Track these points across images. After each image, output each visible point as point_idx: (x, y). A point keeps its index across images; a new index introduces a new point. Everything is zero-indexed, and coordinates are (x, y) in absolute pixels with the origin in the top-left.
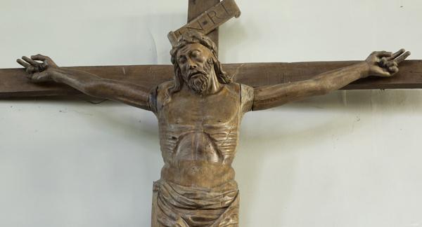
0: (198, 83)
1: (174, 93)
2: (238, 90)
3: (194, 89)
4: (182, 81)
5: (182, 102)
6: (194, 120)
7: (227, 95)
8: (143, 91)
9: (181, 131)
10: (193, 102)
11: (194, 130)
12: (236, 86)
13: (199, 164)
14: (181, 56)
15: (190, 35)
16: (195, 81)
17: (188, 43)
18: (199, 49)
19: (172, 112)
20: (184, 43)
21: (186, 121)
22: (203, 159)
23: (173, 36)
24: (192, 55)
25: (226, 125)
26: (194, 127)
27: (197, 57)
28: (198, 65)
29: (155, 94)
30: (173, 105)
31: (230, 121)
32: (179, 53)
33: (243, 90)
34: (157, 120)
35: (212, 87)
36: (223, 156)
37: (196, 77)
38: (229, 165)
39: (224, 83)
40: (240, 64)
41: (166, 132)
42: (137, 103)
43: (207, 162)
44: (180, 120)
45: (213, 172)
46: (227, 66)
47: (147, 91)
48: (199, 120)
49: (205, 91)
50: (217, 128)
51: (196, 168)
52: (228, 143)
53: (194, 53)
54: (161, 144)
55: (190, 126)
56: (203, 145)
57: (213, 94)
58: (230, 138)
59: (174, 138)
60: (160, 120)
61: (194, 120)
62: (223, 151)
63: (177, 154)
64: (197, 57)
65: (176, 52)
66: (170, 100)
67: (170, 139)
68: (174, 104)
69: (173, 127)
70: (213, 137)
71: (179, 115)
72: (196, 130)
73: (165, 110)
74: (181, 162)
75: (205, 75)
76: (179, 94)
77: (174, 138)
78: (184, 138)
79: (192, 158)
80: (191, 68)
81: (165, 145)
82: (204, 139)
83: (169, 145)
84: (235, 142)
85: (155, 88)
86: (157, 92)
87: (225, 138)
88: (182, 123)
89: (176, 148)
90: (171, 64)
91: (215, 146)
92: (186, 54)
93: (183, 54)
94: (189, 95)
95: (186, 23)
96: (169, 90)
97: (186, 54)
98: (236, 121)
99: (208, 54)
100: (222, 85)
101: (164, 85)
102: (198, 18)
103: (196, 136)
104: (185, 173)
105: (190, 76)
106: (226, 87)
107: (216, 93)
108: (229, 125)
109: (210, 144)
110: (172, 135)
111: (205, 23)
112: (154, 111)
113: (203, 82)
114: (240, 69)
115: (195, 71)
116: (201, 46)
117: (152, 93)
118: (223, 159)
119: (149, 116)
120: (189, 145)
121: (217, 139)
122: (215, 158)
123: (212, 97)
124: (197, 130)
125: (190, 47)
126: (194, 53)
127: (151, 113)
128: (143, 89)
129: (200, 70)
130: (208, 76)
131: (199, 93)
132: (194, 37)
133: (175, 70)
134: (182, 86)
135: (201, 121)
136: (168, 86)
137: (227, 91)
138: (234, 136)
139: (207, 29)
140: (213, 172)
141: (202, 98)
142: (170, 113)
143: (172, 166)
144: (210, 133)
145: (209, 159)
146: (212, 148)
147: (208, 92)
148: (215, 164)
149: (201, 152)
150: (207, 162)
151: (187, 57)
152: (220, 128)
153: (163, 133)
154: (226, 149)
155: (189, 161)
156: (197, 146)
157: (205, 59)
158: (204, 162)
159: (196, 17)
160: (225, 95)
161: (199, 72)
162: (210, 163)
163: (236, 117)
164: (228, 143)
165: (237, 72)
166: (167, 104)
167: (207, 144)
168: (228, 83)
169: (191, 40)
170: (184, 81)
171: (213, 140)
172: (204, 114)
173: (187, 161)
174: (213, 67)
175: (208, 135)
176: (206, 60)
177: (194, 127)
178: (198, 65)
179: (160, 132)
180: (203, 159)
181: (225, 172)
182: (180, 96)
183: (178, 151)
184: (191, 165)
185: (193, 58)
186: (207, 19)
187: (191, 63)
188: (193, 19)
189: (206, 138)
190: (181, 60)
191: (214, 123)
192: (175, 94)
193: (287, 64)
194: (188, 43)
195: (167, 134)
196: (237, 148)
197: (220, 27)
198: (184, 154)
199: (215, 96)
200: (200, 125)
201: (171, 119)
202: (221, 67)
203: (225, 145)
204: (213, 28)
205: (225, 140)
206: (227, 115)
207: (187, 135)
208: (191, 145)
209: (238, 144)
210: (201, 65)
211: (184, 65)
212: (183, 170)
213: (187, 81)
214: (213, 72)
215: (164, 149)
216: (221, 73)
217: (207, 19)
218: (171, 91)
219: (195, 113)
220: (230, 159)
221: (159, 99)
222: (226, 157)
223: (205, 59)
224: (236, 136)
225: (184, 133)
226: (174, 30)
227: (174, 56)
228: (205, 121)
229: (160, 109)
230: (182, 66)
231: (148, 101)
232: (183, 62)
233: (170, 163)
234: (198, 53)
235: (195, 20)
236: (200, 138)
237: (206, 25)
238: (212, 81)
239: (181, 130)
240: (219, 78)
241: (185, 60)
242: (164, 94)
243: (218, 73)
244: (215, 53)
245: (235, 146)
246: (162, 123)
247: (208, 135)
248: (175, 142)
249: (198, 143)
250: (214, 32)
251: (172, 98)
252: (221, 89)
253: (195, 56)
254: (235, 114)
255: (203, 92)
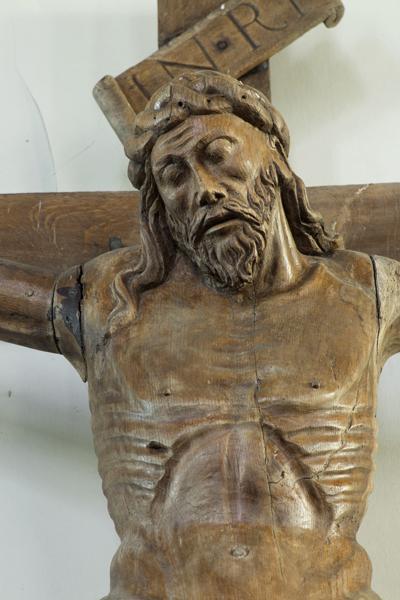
0: (231, 253)
1: (143, 290)
2: (368, 277)
3: (215, 276)
4: (169, 247)
5: (173, 322)
6: (222, 384)
7: (332, 293)
8: (31, 282)
9: (181, 424)
10: (212, 321)
11: (227, 417)
12: (358, 263)
13: (250, 537)
14: (169, 160)
15: (199, 86)
16: (221, 245)
17: (192, 112)
18: (231, 134)
19: (144, 355)
20: (178, 112)
21: (196, 385)
22: (261, 521)
23: (125, 92)
24: (207, 155)
25: (332, 397)
26: (225, 406)
27: (227, 163)
28: (229, 190)
29: (76, 293)
30: (145, 334)
31: (350, 384)
32: (160, 150)
33: (382, 275)
34: (83, 389)
35: (276, 265)
36: (330, 509)
37: (223, 233)
38: (350, 538)
39: (315, 254)
40: (352, 189)
41: (126, 426)
42: (11, 327)
43: (276, 530)
44: (174, 383)
45: (299, 564)
46: (336, 196)
47: (44, 282)
48: (241, 382)
49: (255, 282)
50: (306, 410)
51: (240, 551)
52: (345, 460)
53: (213, 146)
54: (103, 473)
55: (213, 403)
56: (263, 474)
57: (280, 292)
58: (353, 445)
59: (155, 448)
60: (97, 387)
61: (222, 384)
62: (329, 489)
63: (168, 503)
64: (227, 163)
65: (149, 148)
66: (130, 313)
67: (140, 451)
68: (146, 327)
69: (148, 408)
70: (291, 439)
71: (170, 366)
72: (233, 418)
73: (117, 348)
74: (186, 535)
75: (254, 223)
76: (159, 293)
77: (155, 448)
78: (195, 446)
79: (222, 515)
80: (206, 201)
81: (125, 472)
82: (264, 450)
83: (140, 474)
84: (368, 459)
85: (70, 271)
86: (81, 288)
87: (335, 446)
88: (185, 395)
89: (165, 483)
90: (129, 187)
91: (302, 472)
92: (187, 151)
93: (178, 153)
94: (197, 298)
95: (155, 47)
96: (125, 280)
97: (187, 151)
98: (367, 386)
99: (263, 149)
100: (309, 261)
101: (105, 263)
102: (197, 29)
103: (234, 439)
104: (204, 570)
105: (203, 229)
106: (325, 266)
107: (293, 288)
108: (348, 400)
109: (287, 467)
110: (145, 438)
111: (223, 45)
112: (70, 354)
113: (248, 249)
114: (354, 205)
115: (220, 211)
116: (239, 121)
117: (63, 291)
118: (331, 518)
119: (53, 370)
120: (213, 471)
121: (309, 449)
122: (303, 515)
123: (280, 301)
124: (236, 418)
125: (199, 128)
126: (213, 146)
127: (56, 365)
128: (32, 278)
129: (238, 209)
130: (264, 227)
131: (232, 288)
132: (211, 92)
133: (145, 211)
134: (169, 265)
135: (249, 385)
136: (121, 265)
137: (331, 281)
138: (364, 437)
139: (242, 54)
140: (299, 564)
141: (244, 305)
142: (136, 358)
143: (152, 547)
144: (284, 428)
145: (281, 517)
146: (291, 479)
147: (263, 286)
148: (304, 537)
149: (254, 493)
150: (276, 530)
151: (192, 163)
152: (318, 408)
153: (109, 429)
154: (338, 483)
155: (214, 527)
156: (242, 474)
157: (252, 167)
158: (267, 529)
159: (205, 14)
160: (323, 292)
161: (233, 215)
162: (287, 532)
163: (368, 370)
164: (345, 460)
165: (346, 215)
166: (123, 330)
167: (274, 466)
168: (329, 252)
169: (201, 102)
170: (175, 245)
171: (294, 452)
172: (256, 364)
173: (205, 526)
174: (277, 193)
175: (279, 436)
176: (255, 174)
177: (225, 406)
178: (229, 190)
179: (97, 430)
180: (261, 521)
181: (339, 565)
182: (166, 298)
183: (173, 492)
184: (224, 538)
185: (211, 168)
186: (229, 30)
187: (205, 183)
188: (178, 33)
189: (268, 445)
190: (168, 171)
191: (295, 393)
192: (148, 294)
193: (49, 351)
194: (192, 112)
195: (131, 434)
196: (373, 479)
197: (271, 60)
198: (193, 501)
199: (288, 297)
200: (249, 402)
201: (139, 381)
202: (306, 199)
203: (335, 467)
204: (250, 64)
205: (330, 452)
206: (338, 363)
207: (201, 434)
208: (218, 469)
209: (375, 466)
210: (242, 189)
211: (180, 189)
212: (195, 560)
213: (190, 246)
214: (278, 214)
215: (118, 490)
216: (305, 217)
217: (229, 30)
218: (134, 281)
219: (226, 358)
220: (353, 519)
221: (91, 310)
222: (340, 510)
223: (252, 167)
224: (371, 438)
225: (191, 430)
226: (115, 72)
227: (140, 162)
228: (261, 388)
229: (98, 348)
230: (170, 194)
231: (52, 317)
232: (176, 181)
233: (142, 533)
234: (229, 149)
235: (186, 36)
236: (247, 446)
237: (228, 55)
238: (276, 246)
239: (180, 419)
240: (297, 235)
241: (182, 174)
242: (107, 293)
243: (298, 218)
244: (282, 146)
245: (366, 471)
246: (106, 396)
247: (279, 436)
248: (158, 460)
249: (243, 462)
250: (256, 74)
251: (138, 307)
252: (308, 274)
253: (218, 158)
254: (363, 364)
255: (249, 285)
